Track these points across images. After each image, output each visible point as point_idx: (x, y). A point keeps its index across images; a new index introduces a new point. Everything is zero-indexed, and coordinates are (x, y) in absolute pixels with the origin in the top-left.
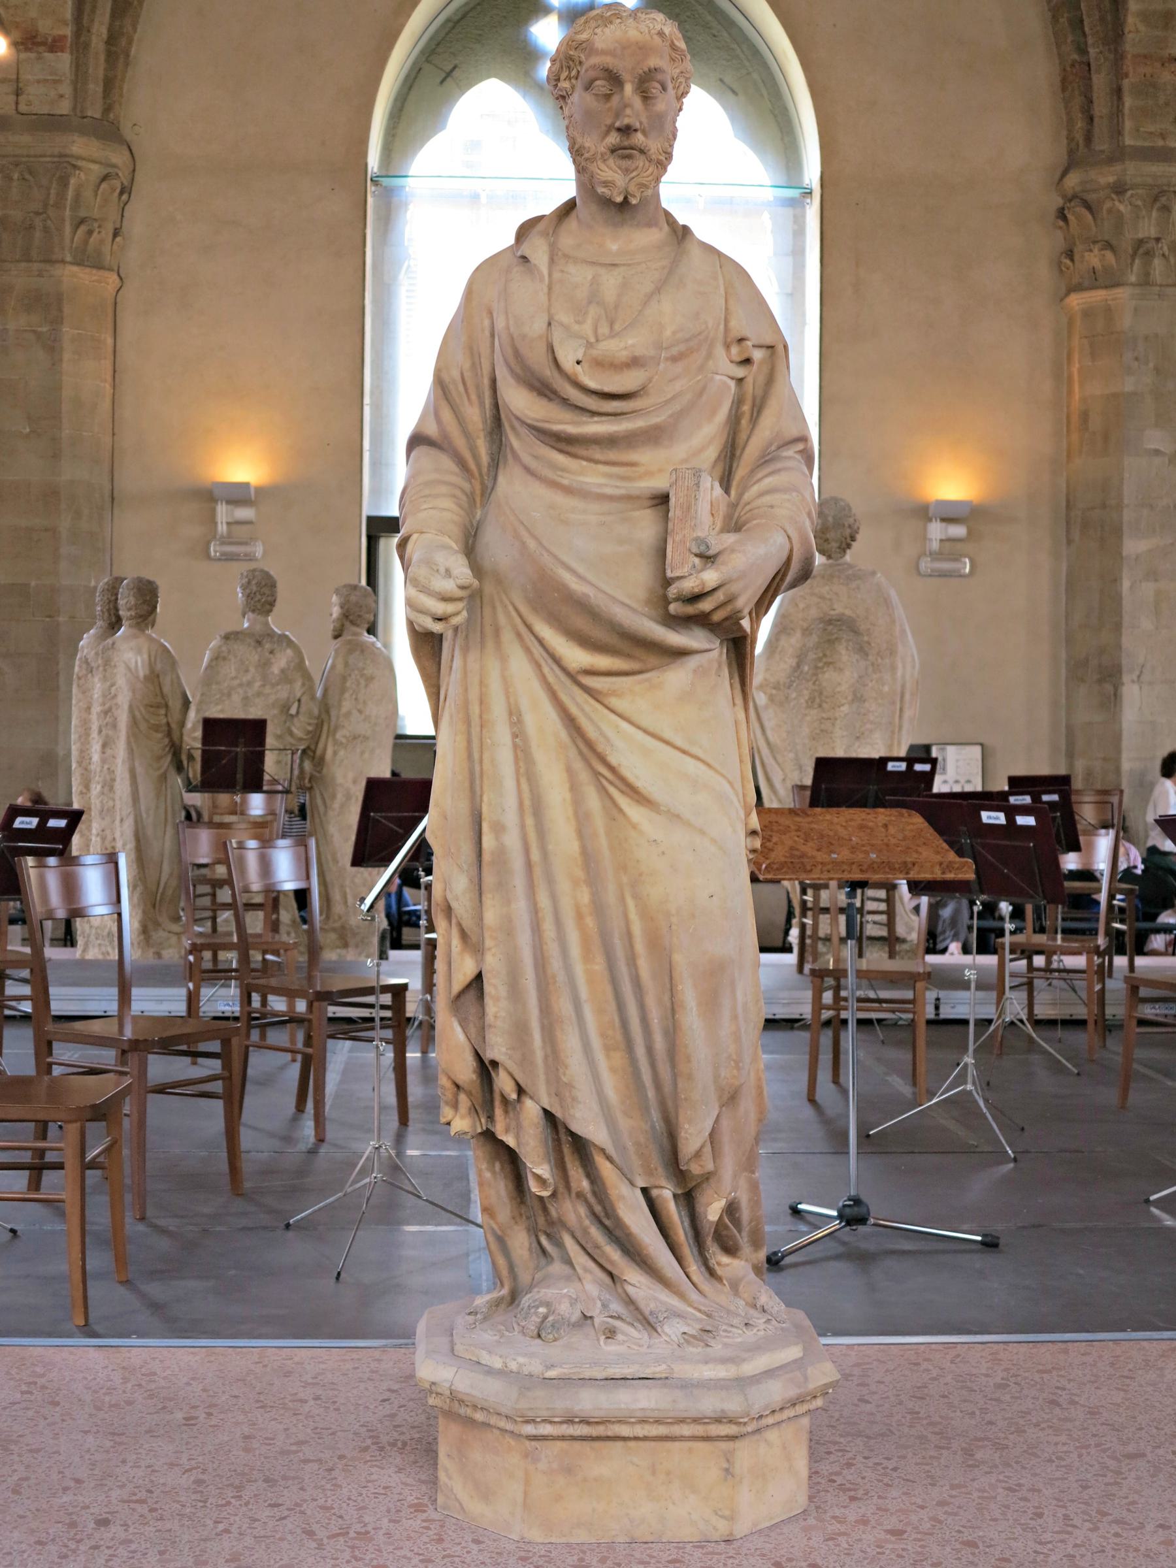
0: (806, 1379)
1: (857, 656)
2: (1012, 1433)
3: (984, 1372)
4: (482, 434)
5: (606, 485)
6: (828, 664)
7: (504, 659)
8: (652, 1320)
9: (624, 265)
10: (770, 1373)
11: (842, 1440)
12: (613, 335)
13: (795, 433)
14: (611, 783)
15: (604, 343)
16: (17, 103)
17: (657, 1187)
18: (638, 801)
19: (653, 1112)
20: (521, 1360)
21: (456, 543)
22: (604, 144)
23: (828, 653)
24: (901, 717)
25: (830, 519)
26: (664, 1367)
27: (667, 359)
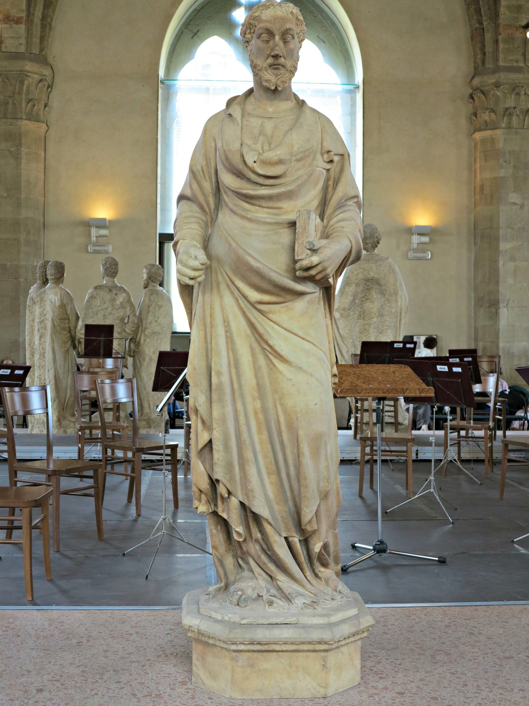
0: (360, 624)
1: (380, 296)
4: (211, 195)
7: (221, 297)
8: (289, 597)
9: (275, 118)
13: (353, 194)
18: (282, 361)
20: (230, 615)
21: (200, 244)
22: (266, 63)
23: (367, 294)
24: (400, 323)
25: (368, 234)
26: (295, 618)
27: (295, 160)
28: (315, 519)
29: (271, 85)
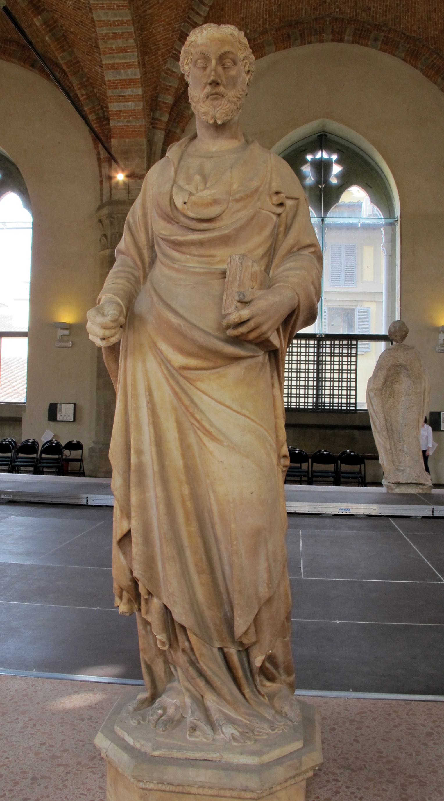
0: (301, 764)
1: (407, 379)
2: (430, 773)
3: (422, 722)
4: (146, 247)
5: (197, 267)
6: (397, 381)
7: (144, 361)
10: (279, 761)
11: (338, 771)
12: (205, 188)
13: (308, 242)
14: (199, 429)
15: (200, 193)
16: (128, 196)
17: (227, 647)
18: (212, 439)
19: (226, 606)
20: (143, 742)
21: (122, 300)
23: (396, 377)
24: (424, 401)
25: (397, 328)
26: (217, 755)
27: (233, 200)
28: (252, 630)
29: (209, 118)
